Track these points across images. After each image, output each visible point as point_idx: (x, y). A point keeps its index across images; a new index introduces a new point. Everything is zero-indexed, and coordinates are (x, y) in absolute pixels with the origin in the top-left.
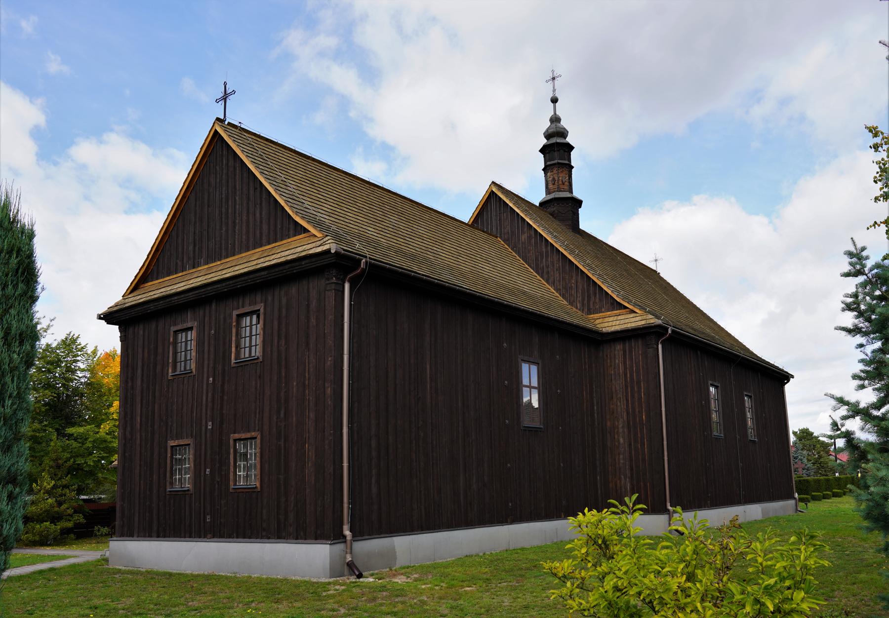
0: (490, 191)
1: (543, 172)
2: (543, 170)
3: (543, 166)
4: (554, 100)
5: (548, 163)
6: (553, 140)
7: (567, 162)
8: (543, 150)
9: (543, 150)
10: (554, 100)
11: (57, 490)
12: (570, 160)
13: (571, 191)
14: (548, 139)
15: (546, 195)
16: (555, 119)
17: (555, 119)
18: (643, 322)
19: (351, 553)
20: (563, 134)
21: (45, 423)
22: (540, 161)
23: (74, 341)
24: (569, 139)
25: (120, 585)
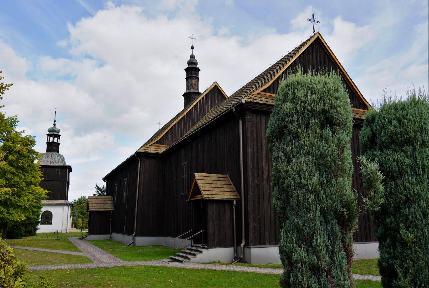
0: (215, 84)
1: (186, 80)
2: (186, 78)
3: (186, 77)
4: (192, 48)
5: (189, 76)
6: (191, 66)
7: (197, 76)
8: (186, 70)
9: (186, 70)
10: (192, 48)
11: (39, 172)
12: (198, 75)
13: (198, 90)
14: (188, 65)
15: (187, 90)
16: (192, 57)
17: (192, 57)
18: (97, 209)
19: (236, 253)
20: (196, 64)
21: (276, 126)
22: (184, 74)
23: (15, 122)
24: (198, 66)
25: (425, 179)
